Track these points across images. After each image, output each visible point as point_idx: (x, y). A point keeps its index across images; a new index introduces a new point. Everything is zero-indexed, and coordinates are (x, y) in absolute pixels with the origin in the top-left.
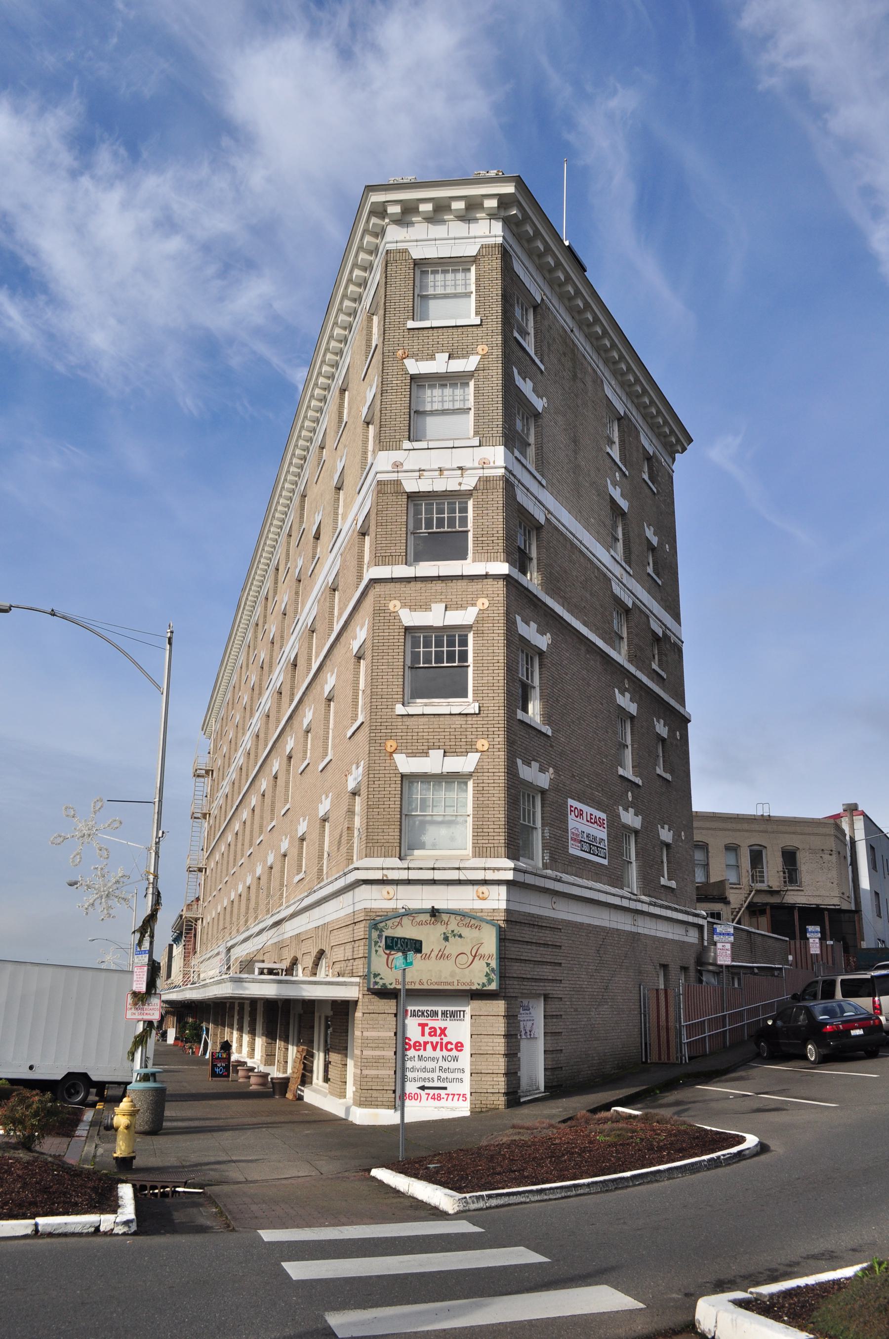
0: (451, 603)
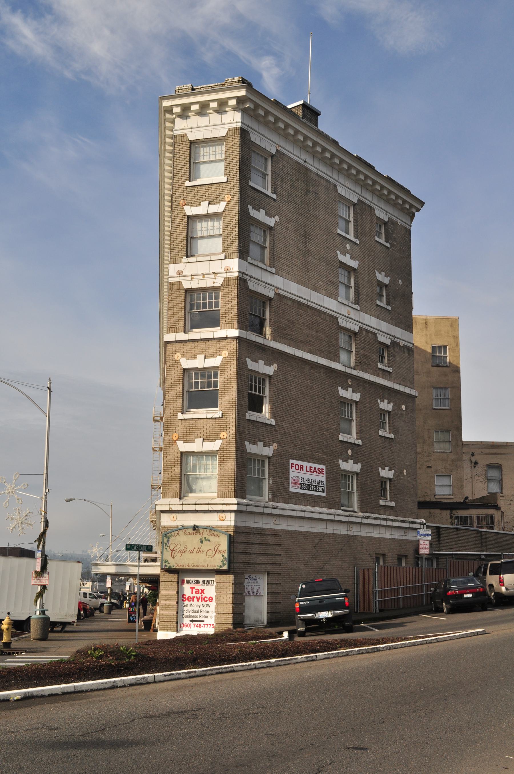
0: (208, 354)
